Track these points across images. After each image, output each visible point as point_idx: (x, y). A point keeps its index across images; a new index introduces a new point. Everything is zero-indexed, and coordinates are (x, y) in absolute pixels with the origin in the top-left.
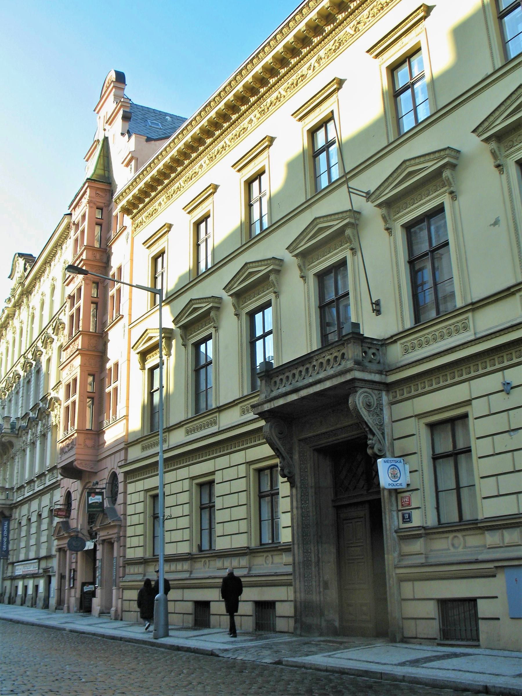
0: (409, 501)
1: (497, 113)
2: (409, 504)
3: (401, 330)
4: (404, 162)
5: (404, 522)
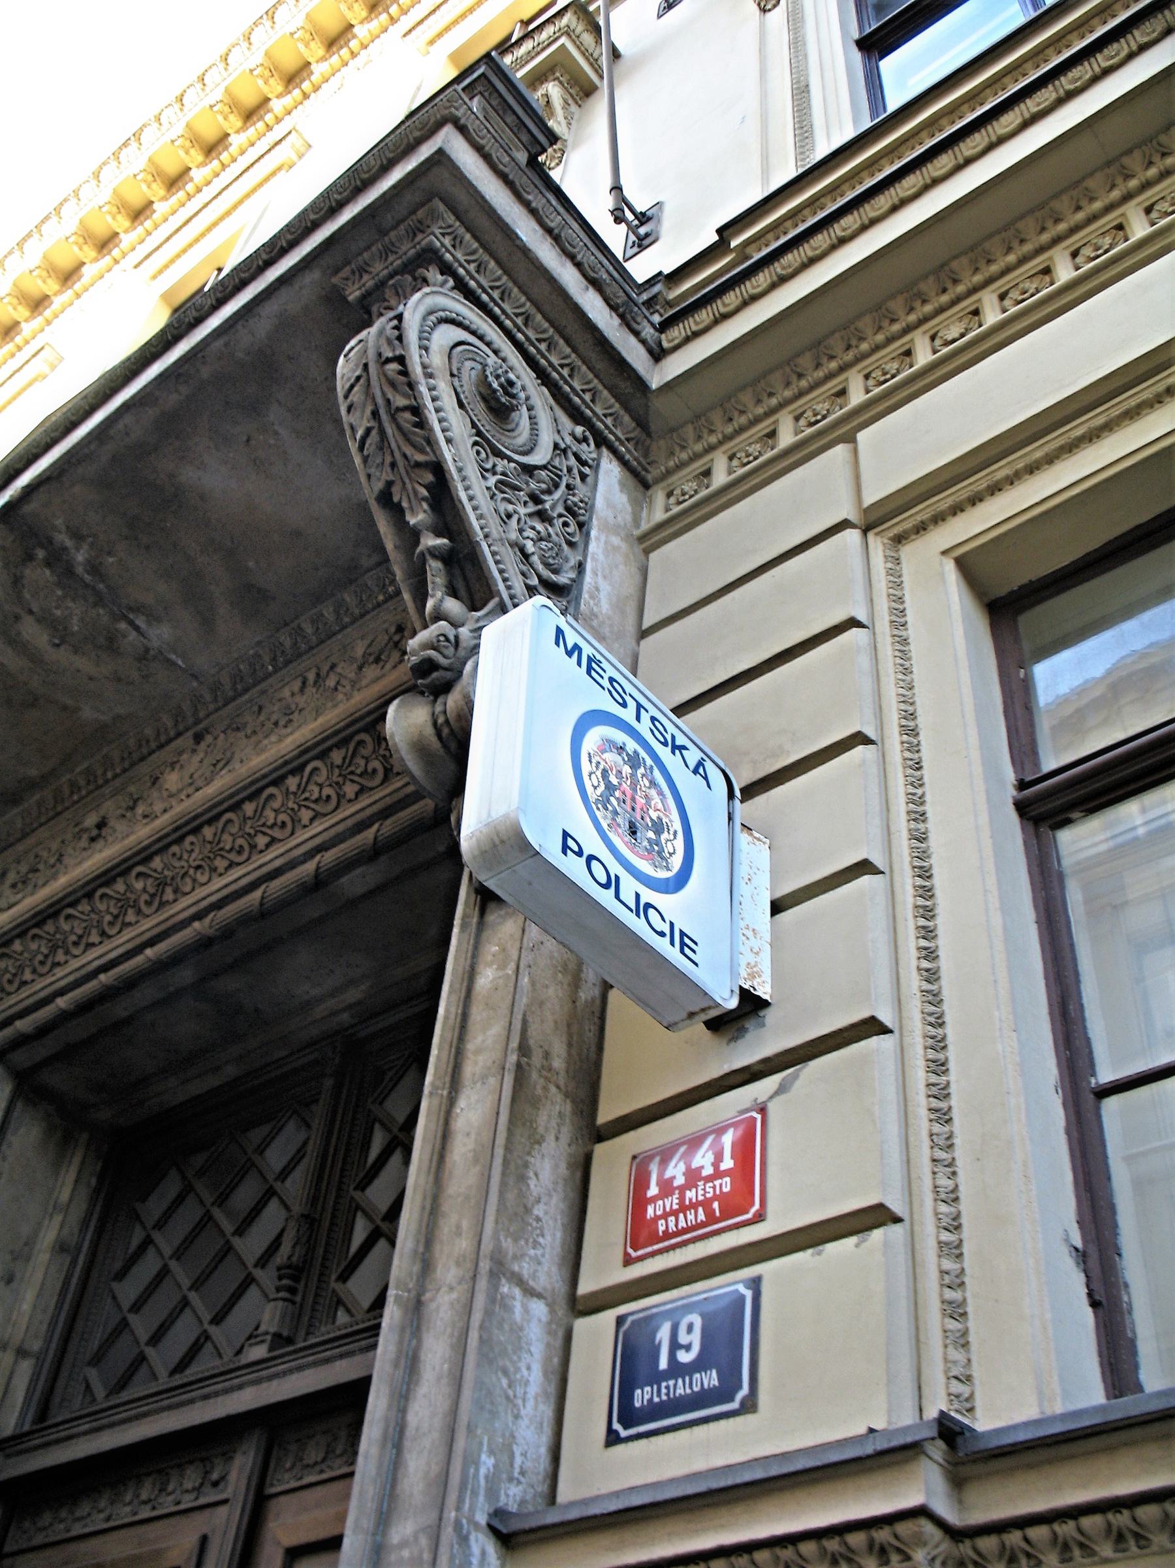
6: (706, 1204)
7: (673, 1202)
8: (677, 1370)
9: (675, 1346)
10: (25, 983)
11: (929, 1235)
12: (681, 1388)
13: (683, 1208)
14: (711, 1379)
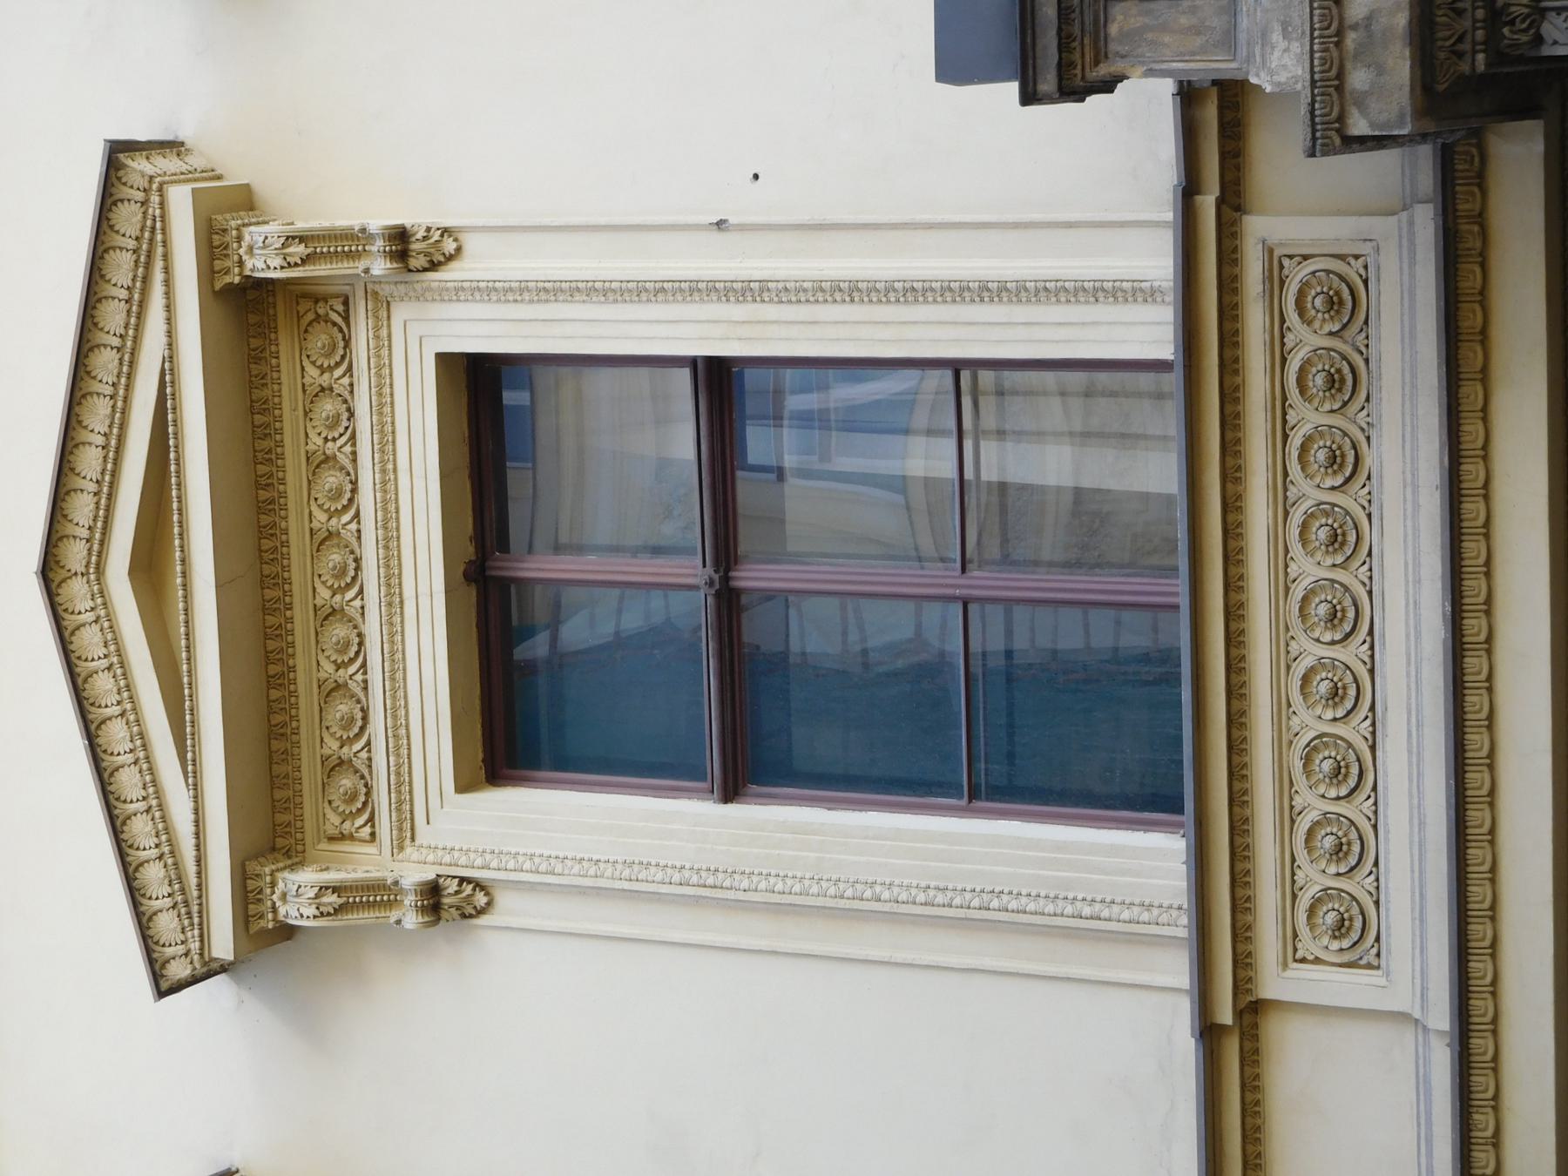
1: (129, 782)
3: (1177, 970)
4: (50, 572)
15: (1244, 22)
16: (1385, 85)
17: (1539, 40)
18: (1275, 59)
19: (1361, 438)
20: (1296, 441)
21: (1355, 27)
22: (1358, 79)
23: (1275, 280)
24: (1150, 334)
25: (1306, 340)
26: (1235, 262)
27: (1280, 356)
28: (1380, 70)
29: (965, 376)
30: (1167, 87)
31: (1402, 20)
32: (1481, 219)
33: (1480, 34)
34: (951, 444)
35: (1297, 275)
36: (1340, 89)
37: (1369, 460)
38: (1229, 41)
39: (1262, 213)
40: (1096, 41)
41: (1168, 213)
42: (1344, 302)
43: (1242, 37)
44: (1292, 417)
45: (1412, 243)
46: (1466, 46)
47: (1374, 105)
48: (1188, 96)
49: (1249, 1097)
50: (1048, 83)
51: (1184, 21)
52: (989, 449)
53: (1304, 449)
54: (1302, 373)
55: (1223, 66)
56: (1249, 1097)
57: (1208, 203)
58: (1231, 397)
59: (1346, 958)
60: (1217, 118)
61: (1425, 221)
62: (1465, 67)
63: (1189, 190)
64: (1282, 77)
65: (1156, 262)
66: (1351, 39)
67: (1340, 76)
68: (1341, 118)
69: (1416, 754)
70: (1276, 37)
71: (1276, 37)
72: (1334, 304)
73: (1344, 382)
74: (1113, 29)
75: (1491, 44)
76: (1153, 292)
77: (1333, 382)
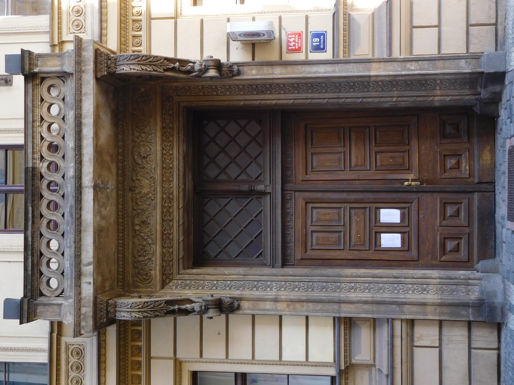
0: (295, 34)
2: (300, 35)
5: (323, 49)
6: (299, 39)
7: (297, 44)
8: (320, 42)
9: (317, 42)
10: (172, 253)
11: (278, 363)
12: (322, 41)
13: (298, 43)
14: (322, 37)
15: (62, 311)
16: (88, 323)
17: (115, 316)
18: (68, 318)
19: (82, 378)
20: (70, 379)
21: (83, 315)
22: (83, 324)
23: (67, 349)
24: (43, 358)
25: (73, 360)
26: (60, 345)
27: (68, 363)
28: (87, 323)
29: (10, 153)
30: (47, 323)
31: (91, 314)
32: (105, 341)
33: (105, 315)
34: (4, 374)
35: (71, 348)
36: (80, 326)
37: (84, 382)
38: (60, 314)
39: (65, 336)
40: (34, 313)
41: (47, 336)
42: (80, 353)
43: (62, 314)
44: (69, 374)
45: (92, 344)
46: (103, 317)
47: (86, 329)
48: (52, 323)
49: (60, 21)
50: (25, 320)
51: (51, 310)
52: (11, 375)
53: (72, 380)
54: (72, 366)
55: (59, 319)
56: (60, 21)
57: (55, 335)
58: (58, 370)
59: (79, 31)
60: (57, 329)
61: (95, 339)
62: (102, 321)
63: (52, 332)
64: (69, 322)
65: (45, 345)
66: (82, 317)
67: (80, 323)
68: (80, 331)
69: (92, 360)
70: (68, 314)
71: (68, 314)
72: (78, 354)
73: (79, 368)
74: (38, 311)
75: (107, 317)
76: (44, 350)
77: (77, 368)
